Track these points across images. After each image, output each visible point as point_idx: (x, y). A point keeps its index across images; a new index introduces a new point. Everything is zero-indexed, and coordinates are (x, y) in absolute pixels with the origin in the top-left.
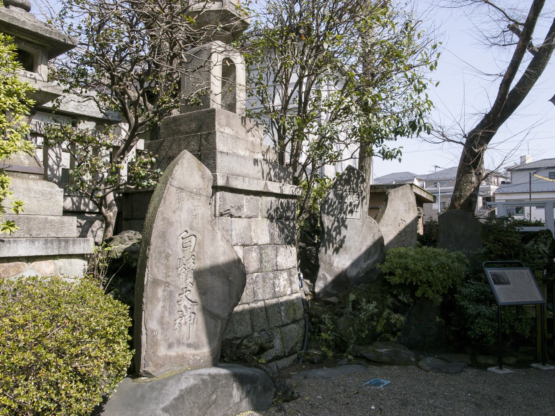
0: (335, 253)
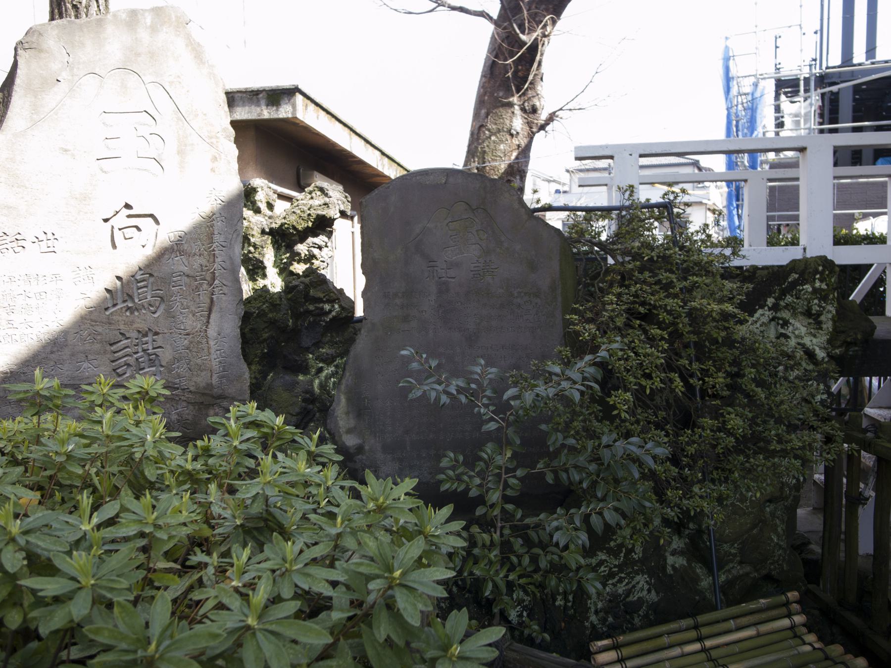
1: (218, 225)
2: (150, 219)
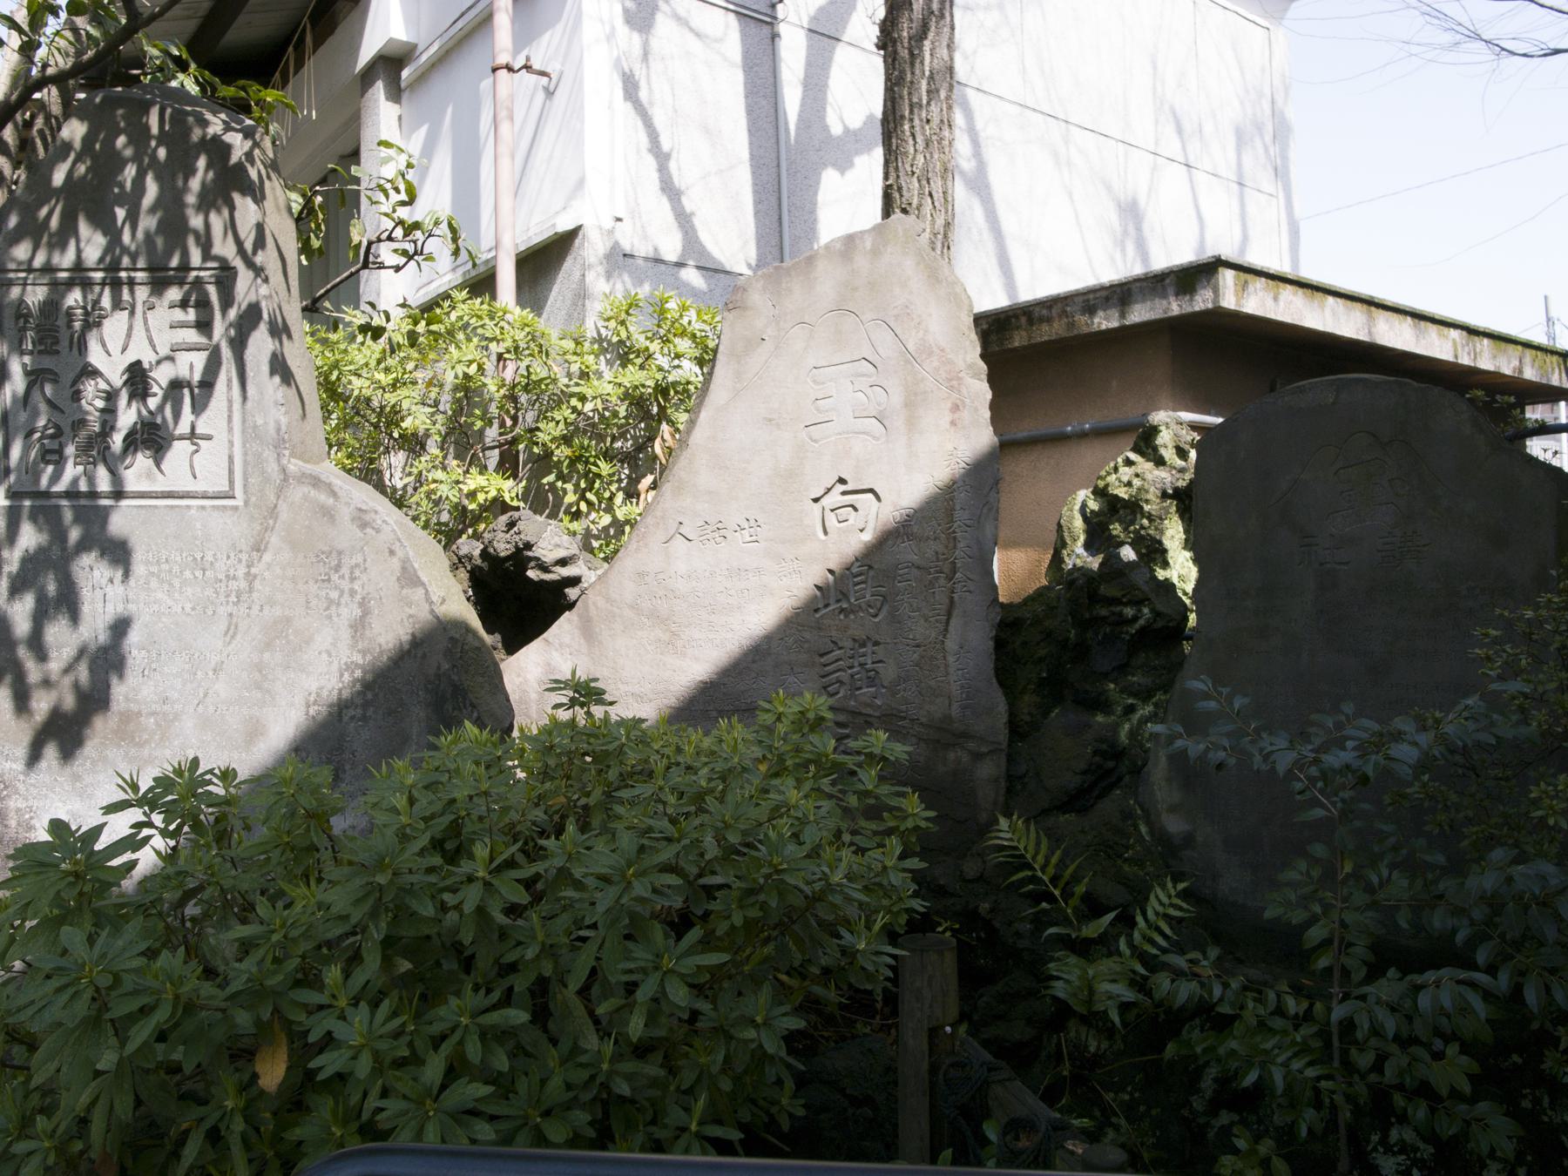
0: (51, 752)
1: (961, 497)
2: (870, 495)
